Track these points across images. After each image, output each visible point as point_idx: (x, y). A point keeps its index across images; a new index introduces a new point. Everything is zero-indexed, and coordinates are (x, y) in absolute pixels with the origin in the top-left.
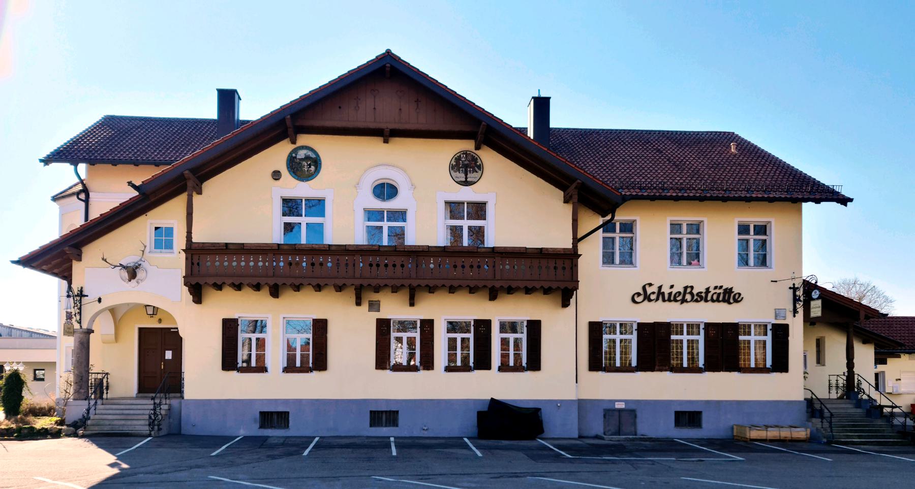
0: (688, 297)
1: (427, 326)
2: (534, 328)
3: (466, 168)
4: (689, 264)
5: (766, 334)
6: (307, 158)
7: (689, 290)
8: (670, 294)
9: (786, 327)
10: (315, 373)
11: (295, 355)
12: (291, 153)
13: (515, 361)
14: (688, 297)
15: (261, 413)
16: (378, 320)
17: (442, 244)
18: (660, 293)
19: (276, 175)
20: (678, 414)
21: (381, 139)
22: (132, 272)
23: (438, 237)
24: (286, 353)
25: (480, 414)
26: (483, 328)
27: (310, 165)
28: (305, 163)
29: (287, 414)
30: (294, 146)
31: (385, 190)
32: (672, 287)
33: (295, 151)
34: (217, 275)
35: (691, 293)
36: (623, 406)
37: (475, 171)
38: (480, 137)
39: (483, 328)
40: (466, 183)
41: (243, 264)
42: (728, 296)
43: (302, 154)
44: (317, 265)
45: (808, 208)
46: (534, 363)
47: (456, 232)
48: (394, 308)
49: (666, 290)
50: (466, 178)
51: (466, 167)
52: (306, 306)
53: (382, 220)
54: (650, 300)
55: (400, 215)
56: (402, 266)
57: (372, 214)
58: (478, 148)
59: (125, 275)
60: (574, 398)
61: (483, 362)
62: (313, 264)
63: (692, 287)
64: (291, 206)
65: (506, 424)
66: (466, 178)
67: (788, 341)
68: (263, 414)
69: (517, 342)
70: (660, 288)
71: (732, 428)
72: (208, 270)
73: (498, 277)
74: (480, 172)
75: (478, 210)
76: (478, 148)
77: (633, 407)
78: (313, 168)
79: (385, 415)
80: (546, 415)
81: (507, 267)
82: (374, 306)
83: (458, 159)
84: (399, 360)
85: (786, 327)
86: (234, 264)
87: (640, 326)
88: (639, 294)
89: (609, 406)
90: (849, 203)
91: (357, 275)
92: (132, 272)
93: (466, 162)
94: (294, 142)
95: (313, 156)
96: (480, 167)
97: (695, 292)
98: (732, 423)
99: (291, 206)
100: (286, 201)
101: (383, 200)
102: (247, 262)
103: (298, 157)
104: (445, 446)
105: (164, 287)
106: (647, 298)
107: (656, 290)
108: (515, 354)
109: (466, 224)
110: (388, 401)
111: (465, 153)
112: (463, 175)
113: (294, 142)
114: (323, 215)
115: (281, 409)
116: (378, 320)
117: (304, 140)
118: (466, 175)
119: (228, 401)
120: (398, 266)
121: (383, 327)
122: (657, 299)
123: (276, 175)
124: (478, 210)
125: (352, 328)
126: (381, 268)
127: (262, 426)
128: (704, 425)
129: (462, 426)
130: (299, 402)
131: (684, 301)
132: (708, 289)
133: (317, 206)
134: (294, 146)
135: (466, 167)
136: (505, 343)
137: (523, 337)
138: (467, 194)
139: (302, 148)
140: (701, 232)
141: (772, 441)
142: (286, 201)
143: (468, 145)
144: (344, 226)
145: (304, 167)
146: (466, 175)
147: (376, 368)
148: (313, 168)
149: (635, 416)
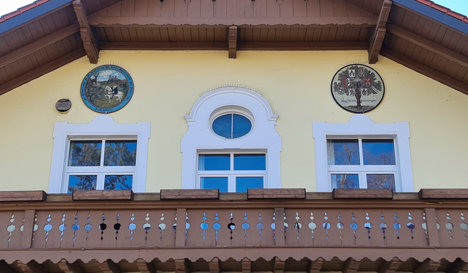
3: (358, 89)
6: (112, 81)
12: (88, 75)
19: (63, 106)
21: (226, 53)
27: (116, 91)
30: (94, 66)
31: (232, 123)
33: (95, 72)
37: (371, 91)
38: (88, 45)
40: (359, 109)
43: (104, 76)
44: (110, 228)
50: (359, 102)
53: (95, 161)
55: (257, 159)
56: (117, 227)
57: (210, 159)
58: (373, 60)
66: (359, 102)
73: (434, 242)
74: (380, 93)
76: (373, 60)
78: (120, 94)
81: (312, 226)
83: (344, 76)
86: (48, 228)
91: (180, 242)
93: (358, 80)
94: (94, 60)
95: (123, 78)
96: (380, 86)
101: (228, 137)
111: (355, 67)
112: (354, 98)
113: (94, 60)
114: (365, 164)
117: (108, 57)
118: (358, 97)
124: (381, 148)
134: (94, 66)
139: (106, 67)
143: (360, 57)
146: (358, 97)
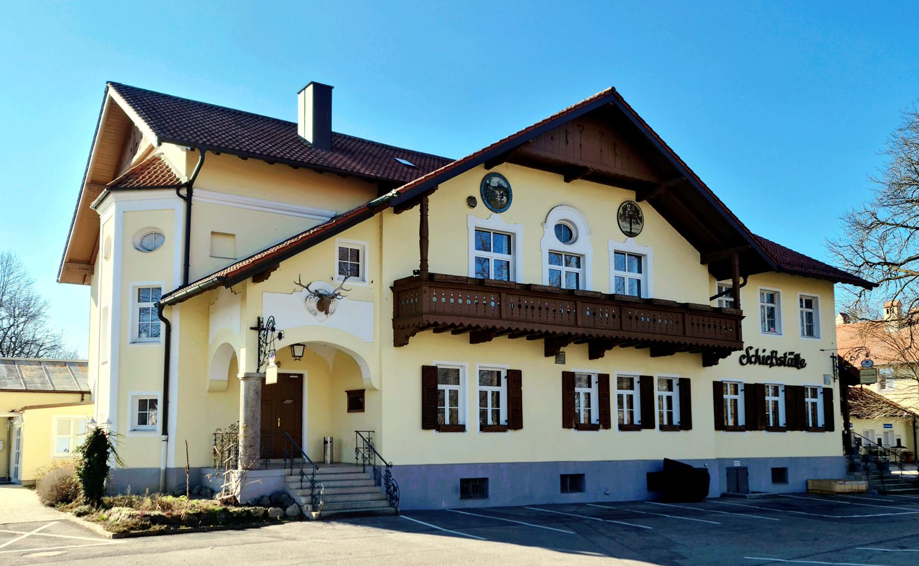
0: (774, 361)
1: (604, 380)
2: (515, 378)
3: (630, 218)
4: (769, 330)
5: (499, 384)
6: (500, 187)
9: (831, 390)
10: (510, 433)
13: (813, 424)
15: (461, 480)
16: (563, 373)
17: (462, 273)
18: (757, 356)
20: (563, 477)
22: (324, 302)
23: (467, 269)
24: (148, 398)
25: (650, 476)
26: (647, 383)
27: (502, 195)
29: (485, 481)
32: (764, 351)
33: (488, 177)
34: (453, 315)
35: (776, 358)
36: (739, 465)
39: (647, 383)
40: (631, 234)
41: (460, 301)
42: (797, 362)
43: (495, 181)
45: (838, 286)
46: (515, 421)
47: (620, 281)
48: (577, 361)
49: (761, 354)
51: (631, 217)
52: (502, 355)
54: (751, 363)
58: (639, 199)
59: (314, 302)
61: (647, 422)
62: (594, 314)
63: (776, 352)
64: (484, 239)
65: (675, 483)
68: (563, 477)
69: (497, 395)
70: (757, 351)
71: (807, 482)
72: (418, 305)
76: (639, 199)
77: (745, 465)
79: (572, 480)
82: (561, 359)
84: (854, 425)
85: (831, 390)
87: (747, 386)
89: (729, 465)
90: (874, 289)
92: (324, 302)
95: (506, 186)
96: (641, 219)
97: (778, 356)
98: (806, 478)
99: (484, 239)
100: (479, 232)
105: (361, 321)
106: (749, 361)
110: (574, 463)
111: (630, 203)
115: (481, 475)
116: (563, 373)
119: (429, 466)
121: (569, 380)
123: (471, 202)
125: (542, 380)
126: (566, 318)
127: (564, 489)
128: (790, 480)
129: (632, 489)
130: (497, 465)
131: (771, 365)
132: (785, 354)
133: (507, 241)
135: (631, 217)
137: (503, 390)
138: (631, 245)
140: (814, 306)
141: (852, 493)
142: (479, 232)
144: (532, 268)
145: (496, 197)
147: (564, 427)
148: (505, 199)
149: (747, 474)
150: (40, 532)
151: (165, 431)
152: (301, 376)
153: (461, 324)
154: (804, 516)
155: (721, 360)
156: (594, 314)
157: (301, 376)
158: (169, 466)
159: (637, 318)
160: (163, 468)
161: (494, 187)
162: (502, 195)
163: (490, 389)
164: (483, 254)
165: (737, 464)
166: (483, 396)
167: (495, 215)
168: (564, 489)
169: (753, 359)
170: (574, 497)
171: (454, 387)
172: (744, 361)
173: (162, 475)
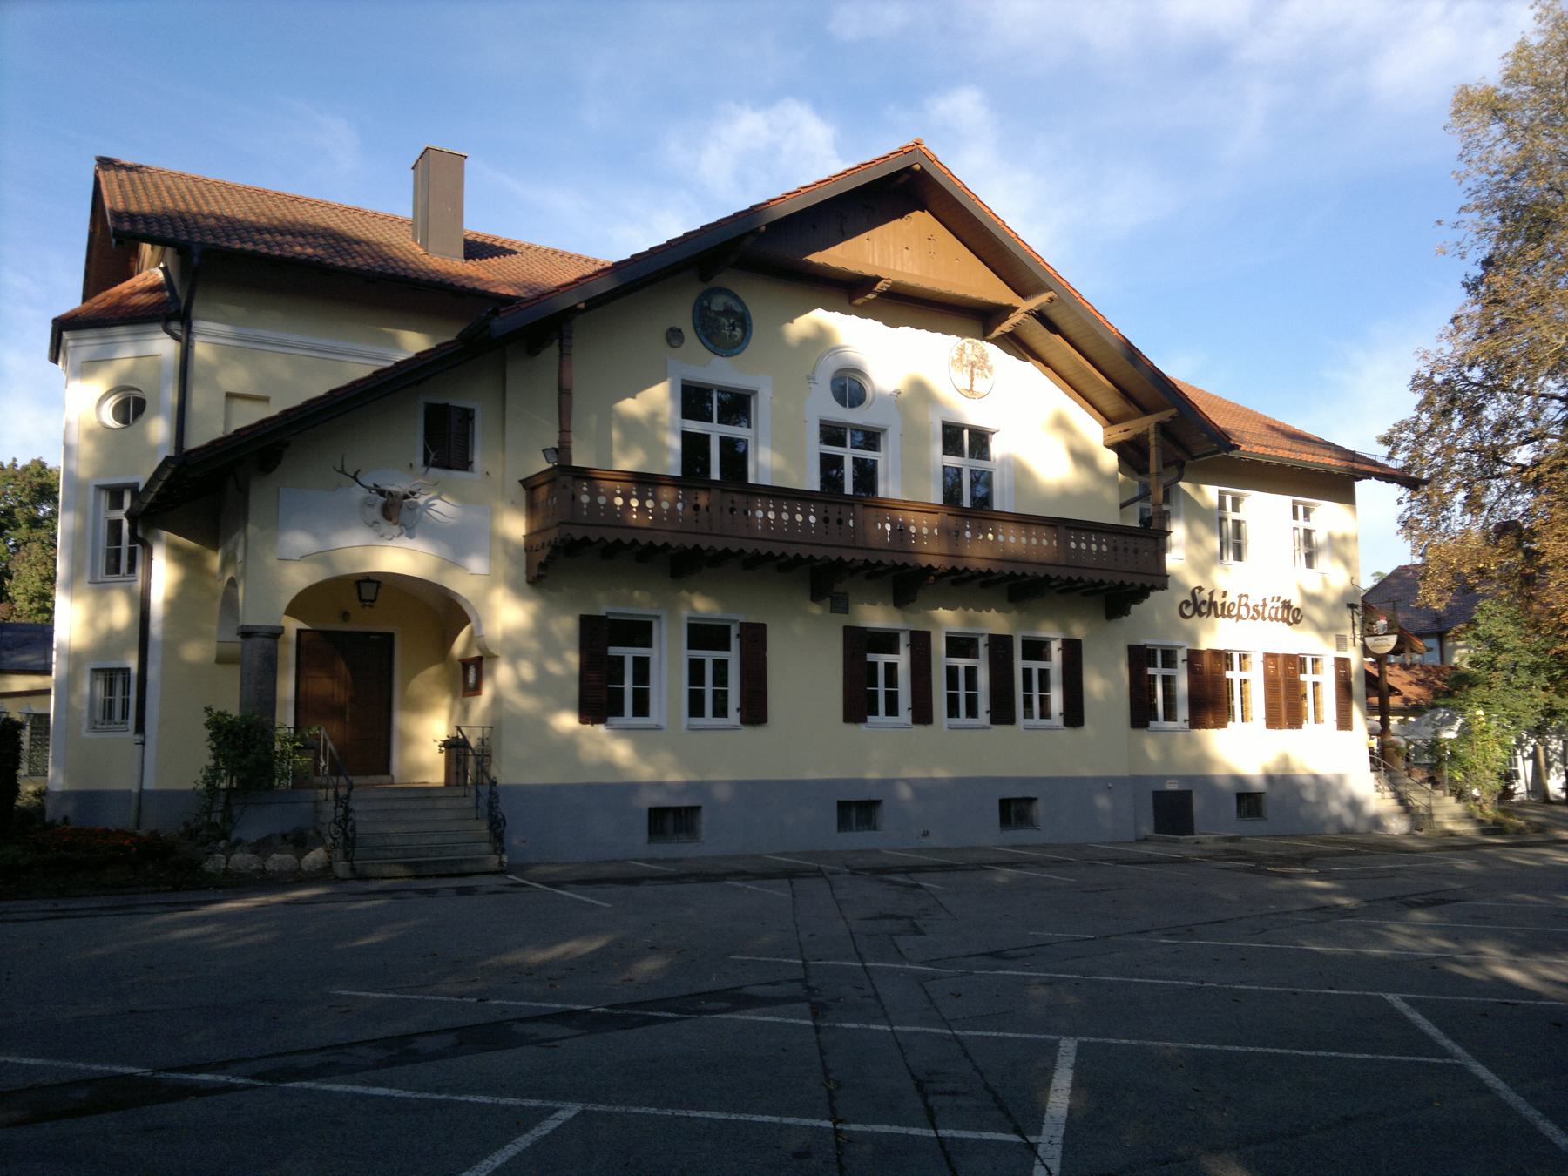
1: (921, 643)
6: (728, 312)
7: (1244, 601)
8: (1223, 604)
11: (876, 692)
14: (1244, 611)
20: (843, 806)
28: (724, 320)
54: (1201, 614)
60: (1126, 774)
62: (826, 520)
67: (764, 659)
70: (1211, 594)
75: (737, 406)
78: (738, 332)
79: (858, 810)
80: (1198, 804)
88: (1187, 603)
95: (739, 309)
102: (792, 514)
103: (713, 307)
104: (683, 876)
107: (1207, 598)
108: (725, 683)
109: (715, 431)
115: (686, 802)
120: (833, 522)
121: (861, 643)
122: (1209, 613)
127: (843, 824)
133: (737, 406)
134: (704, 287)
136: (952, 672)
137: (733, 656)
148: (738, 332)
150: (524, 1119)
151: (140, 727)
152: (390, 636)
153: (1080, 579)
154: (1237, 869)
155: (1134, 608)
156: (826, 520)
157: (390, 636)
158: (146, 787)
159: (840, 522)
160: (135, 790)
161: (719, 313)
162: (733, 325)
163: (709, 656)
164: (695, 426)
165: (1172, 786)
166: (696, 668)
167: (717, 360)
168: (843, 824)
169: (1204, 609)
170: (858, 840)
171: (641, 652)
172: (1188, 612)
173: (134, 802)
